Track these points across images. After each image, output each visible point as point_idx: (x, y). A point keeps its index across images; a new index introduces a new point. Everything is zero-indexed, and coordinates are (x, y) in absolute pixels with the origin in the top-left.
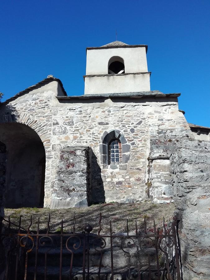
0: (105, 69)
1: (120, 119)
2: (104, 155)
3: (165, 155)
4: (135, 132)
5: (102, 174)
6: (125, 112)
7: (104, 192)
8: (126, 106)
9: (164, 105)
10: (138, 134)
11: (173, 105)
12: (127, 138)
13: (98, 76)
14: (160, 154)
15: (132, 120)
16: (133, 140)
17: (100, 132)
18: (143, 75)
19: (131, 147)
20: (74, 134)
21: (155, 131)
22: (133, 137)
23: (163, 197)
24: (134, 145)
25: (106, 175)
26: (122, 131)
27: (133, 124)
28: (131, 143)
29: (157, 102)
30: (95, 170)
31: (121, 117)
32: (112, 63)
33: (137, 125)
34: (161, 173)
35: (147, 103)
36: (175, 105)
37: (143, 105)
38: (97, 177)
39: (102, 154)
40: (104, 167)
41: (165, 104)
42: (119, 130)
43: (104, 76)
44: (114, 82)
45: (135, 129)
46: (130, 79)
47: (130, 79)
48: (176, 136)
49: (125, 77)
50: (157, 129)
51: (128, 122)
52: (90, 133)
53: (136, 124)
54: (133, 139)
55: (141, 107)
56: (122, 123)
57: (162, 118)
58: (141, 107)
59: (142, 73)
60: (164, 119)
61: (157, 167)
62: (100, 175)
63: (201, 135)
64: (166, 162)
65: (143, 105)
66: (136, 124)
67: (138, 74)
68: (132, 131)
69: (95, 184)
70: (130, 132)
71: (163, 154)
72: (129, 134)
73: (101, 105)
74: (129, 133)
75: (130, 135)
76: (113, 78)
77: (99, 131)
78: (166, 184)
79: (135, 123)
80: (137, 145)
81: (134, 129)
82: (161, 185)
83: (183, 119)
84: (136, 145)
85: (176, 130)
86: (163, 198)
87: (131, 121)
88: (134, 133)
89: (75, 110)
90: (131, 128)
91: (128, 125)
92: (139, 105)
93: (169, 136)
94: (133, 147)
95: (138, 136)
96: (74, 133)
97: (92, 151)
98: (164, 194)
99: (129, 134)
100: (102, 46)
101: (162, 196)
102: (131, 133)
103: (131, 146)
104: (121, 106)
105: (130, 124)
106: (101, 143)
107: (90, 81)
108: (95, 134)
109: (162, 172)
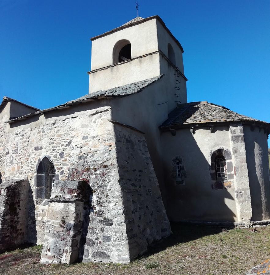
0: (109, 59)
1: (51, 140)
2: (39, 188)
3: (61, 196)
4: (64, 156)
5: (36, 211)
6: (57, 129)
7: (36, 232)
8: (57, 121)
9: (93, 113)
10: (67, 159)
11: (104, 111)
12: (56, 165)
13: (101, 70)
14: (57, 194)
15: (63, 140)
16: (61, 168)
17: (35, 158)
18: (151, 57)
19: (60, 178)
20: (18, 164)
21: (76, 156)
22: (62, 163)
23: (47, 255)
24: (62, 174)
25: (38, 213)
26: (52, 156)
27: (62, 145)
28: (60, 173)
29: (27, 124)
30: (31, 206)
31: (53, 138)
32: (122, 48)
33: (67, 147)
34: (52, 221)
35: (76, 114)
36: (107, 110)
37: (74, 118)
38: (31, 215)
39: (36, 188)
40: (37, 202)
41: (94, 112)
42: (50, 155)
43: (107, 68)
44: (118, 72)
45: (65, 152)
46: (136, 65)
47: (136, 65)
48: (95, 162)
49: (130, 64)
50: (78, 152)
51: (58, 144)
52: (28, 161)
53: (66, 146)
54: (62, 166)
55: (71, 120)
56: (53, 145)
57: (87, 135)
58: (71, 120)
59: (149, 54)
60: (89, 136)
61: (50, 212)
62: (34, 213)
63: (218, 132)
64: (59, 207)
65: (74, 118)
66: (66, 146)
67: (144, 56)
68: (62, 155)
69: (30, 223)
70: (60, 157)
71: (59, 194)
72: (58, 160)
73: (37, 125)
74: (58, 159)
75: (59, 162)
76: (117, 69)
77: (35, 158)
78: (53, 237)
79: (65, 144)
80: (66, 174)
81: (63, 153)
82: (48, 238)
83: (110, 134)
84: (64, 174)
85: (98, 152)
86: (47, 256)
87: (61, 142)
88: (63, 159)
89: (19, 134)
90: (60, 151)
91: (58, 148)
92: (68, 118)
93: (88, 162)
94: (61, 177)
95: (67, 162)
96: (18, 163)
97: (29, 184)
98: (49, 250)
99: (58, 160)
100: (125, 25)
101: (47, 253)
102: (60, 158)
103: (60, 176)
104: (52, 122)
105: (60, 147)
106: (36, 174)
107: (94, 77)
108: (32, 163)
109: (54, 221)
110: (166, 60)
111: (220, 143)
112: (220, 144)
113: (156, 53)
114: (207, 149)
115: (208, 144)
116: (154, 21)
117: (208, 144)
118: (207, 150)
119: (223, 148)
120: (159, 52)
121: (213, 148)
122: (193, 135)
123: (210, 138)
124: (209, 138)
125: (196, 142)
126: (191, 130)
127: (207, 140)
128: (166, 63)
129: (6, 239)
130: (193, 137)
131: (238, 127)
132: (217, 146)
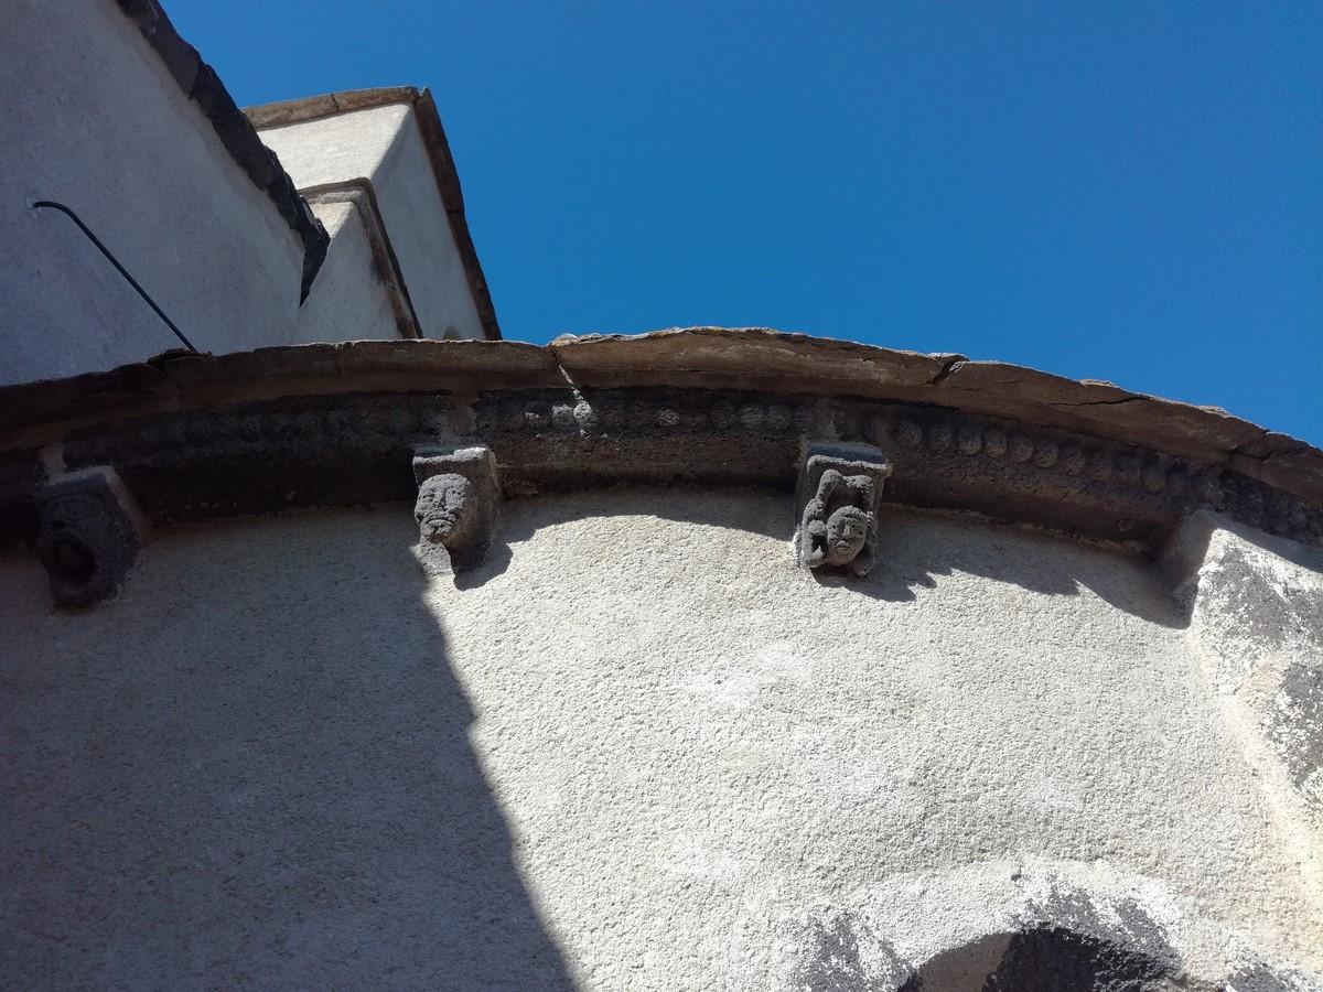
110: (373, 242)
111: (1045, 793)
112: (1048, 831)
113: (329, 195)
114: (727, 867)
115: (762, 777)
116: (396, 114)
117: (762, 777)
118: (705, 897)
119: (1130, 911)
120: (355, 193)
121: (879, 869)
122: (443, 593)
123: (800, 670)
124: (777, 658)
125: (458, 709)
126: (440, 494)
127: (737, 691)
128: (357, 220)
129: (478, 450)
130: (433, 635)
131: (1075, 592)
132: (978, 854)
